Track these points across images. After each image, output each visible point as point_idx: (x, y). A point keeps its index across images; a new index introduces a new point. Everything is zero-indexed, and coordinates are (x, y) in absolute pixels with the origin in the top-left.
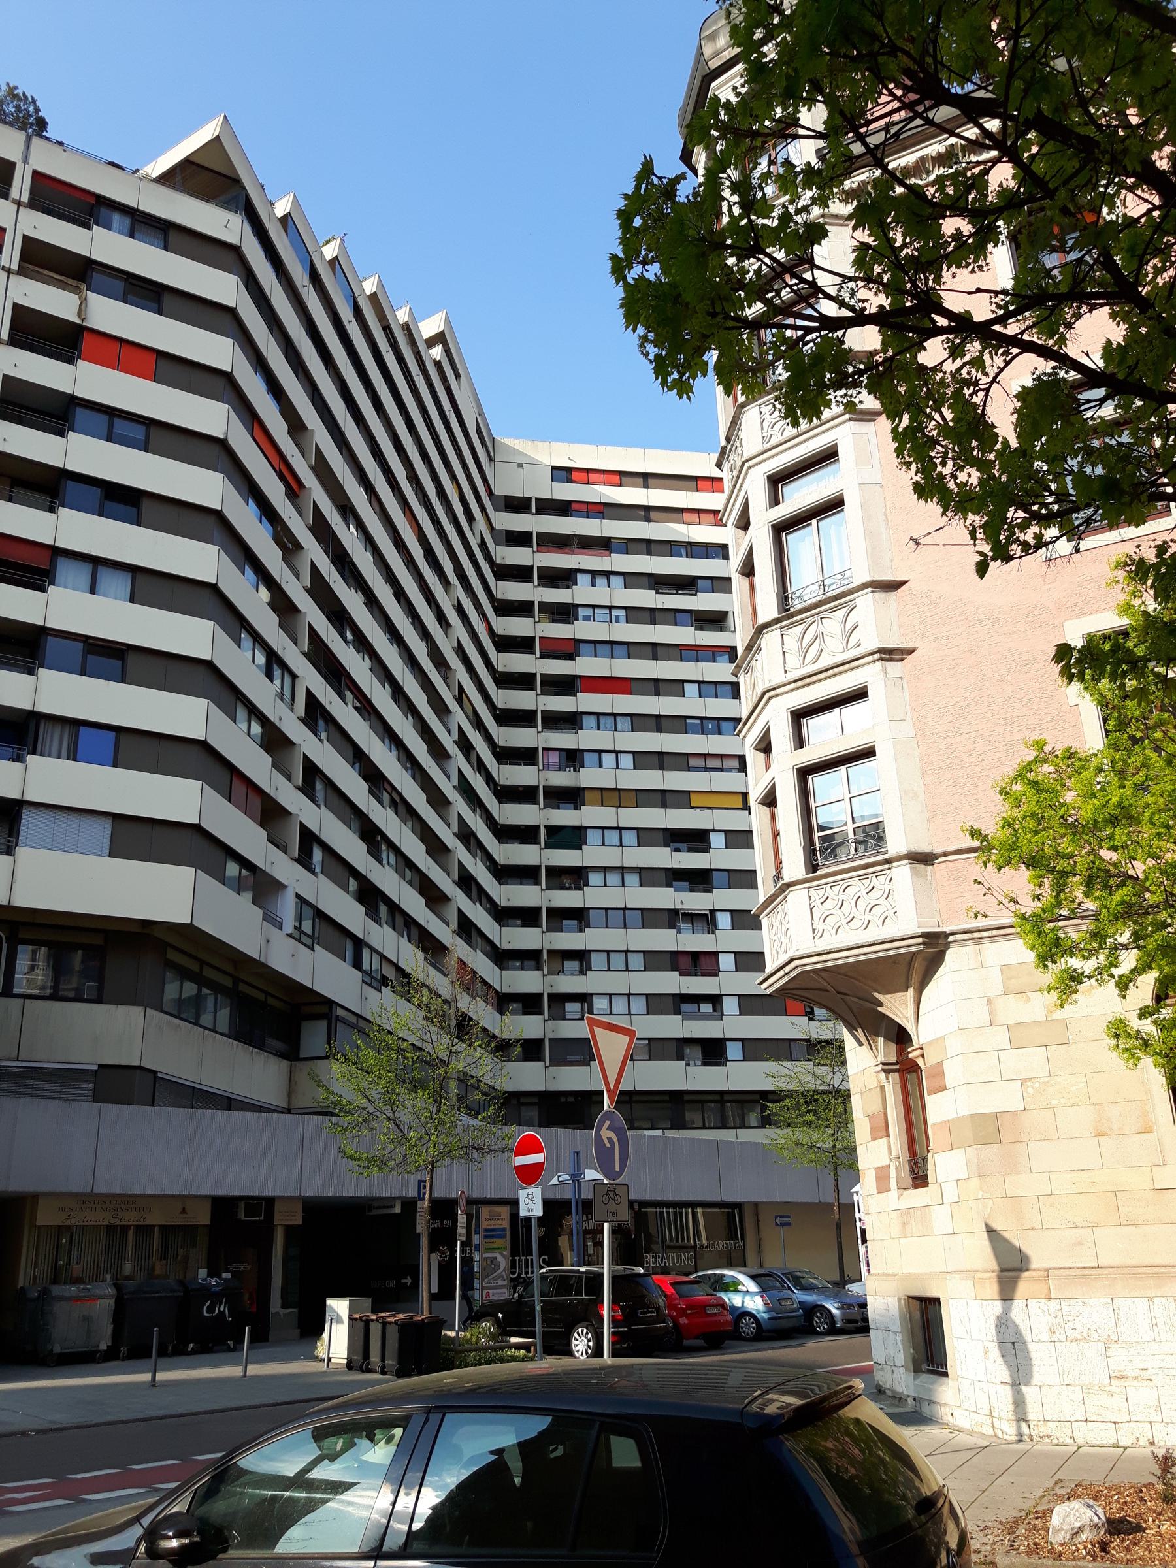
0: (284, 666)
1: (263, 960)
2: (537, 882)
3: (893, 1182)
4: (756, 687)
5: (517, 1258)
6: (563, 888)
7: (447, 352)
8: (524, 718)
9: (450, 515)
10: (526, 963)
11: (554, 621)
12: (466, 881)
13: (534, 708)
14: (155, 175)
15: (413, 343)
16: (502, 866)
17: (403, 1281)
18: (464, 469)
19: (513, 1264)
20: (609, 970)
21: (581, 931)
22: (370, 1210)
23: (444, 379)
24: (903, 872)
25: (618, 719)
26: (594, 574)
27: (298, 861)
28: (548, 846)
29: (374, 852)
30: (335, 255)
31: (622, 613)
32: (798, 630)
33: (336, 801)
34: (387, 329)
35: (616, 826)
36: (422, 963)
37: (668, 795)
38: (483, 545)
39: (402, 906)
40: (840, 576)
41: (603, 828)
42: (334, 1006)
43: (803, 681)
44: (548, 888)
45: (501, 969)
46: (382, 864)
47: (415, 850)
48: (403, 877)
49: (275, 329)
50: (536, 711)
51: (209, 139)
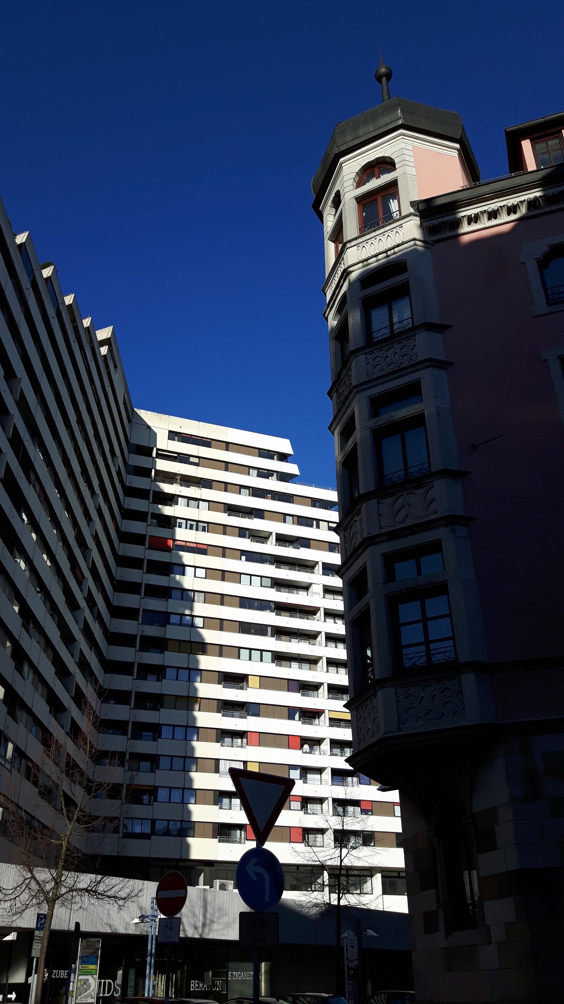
2: (125, 733)
3: (441, 925)
6: (145, 708)
7: (110, 350)
11: (160, 526)
13: (135, 633)
17: (9, 996)
18: (112, 423)
20: (171, 770)
21: (154, 740)
23: (107, 367)
26: (189, 498)
28: (148, 572)
29: (19, 669)
30: (48, 276)
31: (184, 522)
32: (389, 500)
35: (186, 667)
37: (225, 597)
38: (119, 473)
40: (420, 467)
41: (178, 668)
43: (392, 535)
46: (23, 678)
47: (54, 634)
48: (36, 689)
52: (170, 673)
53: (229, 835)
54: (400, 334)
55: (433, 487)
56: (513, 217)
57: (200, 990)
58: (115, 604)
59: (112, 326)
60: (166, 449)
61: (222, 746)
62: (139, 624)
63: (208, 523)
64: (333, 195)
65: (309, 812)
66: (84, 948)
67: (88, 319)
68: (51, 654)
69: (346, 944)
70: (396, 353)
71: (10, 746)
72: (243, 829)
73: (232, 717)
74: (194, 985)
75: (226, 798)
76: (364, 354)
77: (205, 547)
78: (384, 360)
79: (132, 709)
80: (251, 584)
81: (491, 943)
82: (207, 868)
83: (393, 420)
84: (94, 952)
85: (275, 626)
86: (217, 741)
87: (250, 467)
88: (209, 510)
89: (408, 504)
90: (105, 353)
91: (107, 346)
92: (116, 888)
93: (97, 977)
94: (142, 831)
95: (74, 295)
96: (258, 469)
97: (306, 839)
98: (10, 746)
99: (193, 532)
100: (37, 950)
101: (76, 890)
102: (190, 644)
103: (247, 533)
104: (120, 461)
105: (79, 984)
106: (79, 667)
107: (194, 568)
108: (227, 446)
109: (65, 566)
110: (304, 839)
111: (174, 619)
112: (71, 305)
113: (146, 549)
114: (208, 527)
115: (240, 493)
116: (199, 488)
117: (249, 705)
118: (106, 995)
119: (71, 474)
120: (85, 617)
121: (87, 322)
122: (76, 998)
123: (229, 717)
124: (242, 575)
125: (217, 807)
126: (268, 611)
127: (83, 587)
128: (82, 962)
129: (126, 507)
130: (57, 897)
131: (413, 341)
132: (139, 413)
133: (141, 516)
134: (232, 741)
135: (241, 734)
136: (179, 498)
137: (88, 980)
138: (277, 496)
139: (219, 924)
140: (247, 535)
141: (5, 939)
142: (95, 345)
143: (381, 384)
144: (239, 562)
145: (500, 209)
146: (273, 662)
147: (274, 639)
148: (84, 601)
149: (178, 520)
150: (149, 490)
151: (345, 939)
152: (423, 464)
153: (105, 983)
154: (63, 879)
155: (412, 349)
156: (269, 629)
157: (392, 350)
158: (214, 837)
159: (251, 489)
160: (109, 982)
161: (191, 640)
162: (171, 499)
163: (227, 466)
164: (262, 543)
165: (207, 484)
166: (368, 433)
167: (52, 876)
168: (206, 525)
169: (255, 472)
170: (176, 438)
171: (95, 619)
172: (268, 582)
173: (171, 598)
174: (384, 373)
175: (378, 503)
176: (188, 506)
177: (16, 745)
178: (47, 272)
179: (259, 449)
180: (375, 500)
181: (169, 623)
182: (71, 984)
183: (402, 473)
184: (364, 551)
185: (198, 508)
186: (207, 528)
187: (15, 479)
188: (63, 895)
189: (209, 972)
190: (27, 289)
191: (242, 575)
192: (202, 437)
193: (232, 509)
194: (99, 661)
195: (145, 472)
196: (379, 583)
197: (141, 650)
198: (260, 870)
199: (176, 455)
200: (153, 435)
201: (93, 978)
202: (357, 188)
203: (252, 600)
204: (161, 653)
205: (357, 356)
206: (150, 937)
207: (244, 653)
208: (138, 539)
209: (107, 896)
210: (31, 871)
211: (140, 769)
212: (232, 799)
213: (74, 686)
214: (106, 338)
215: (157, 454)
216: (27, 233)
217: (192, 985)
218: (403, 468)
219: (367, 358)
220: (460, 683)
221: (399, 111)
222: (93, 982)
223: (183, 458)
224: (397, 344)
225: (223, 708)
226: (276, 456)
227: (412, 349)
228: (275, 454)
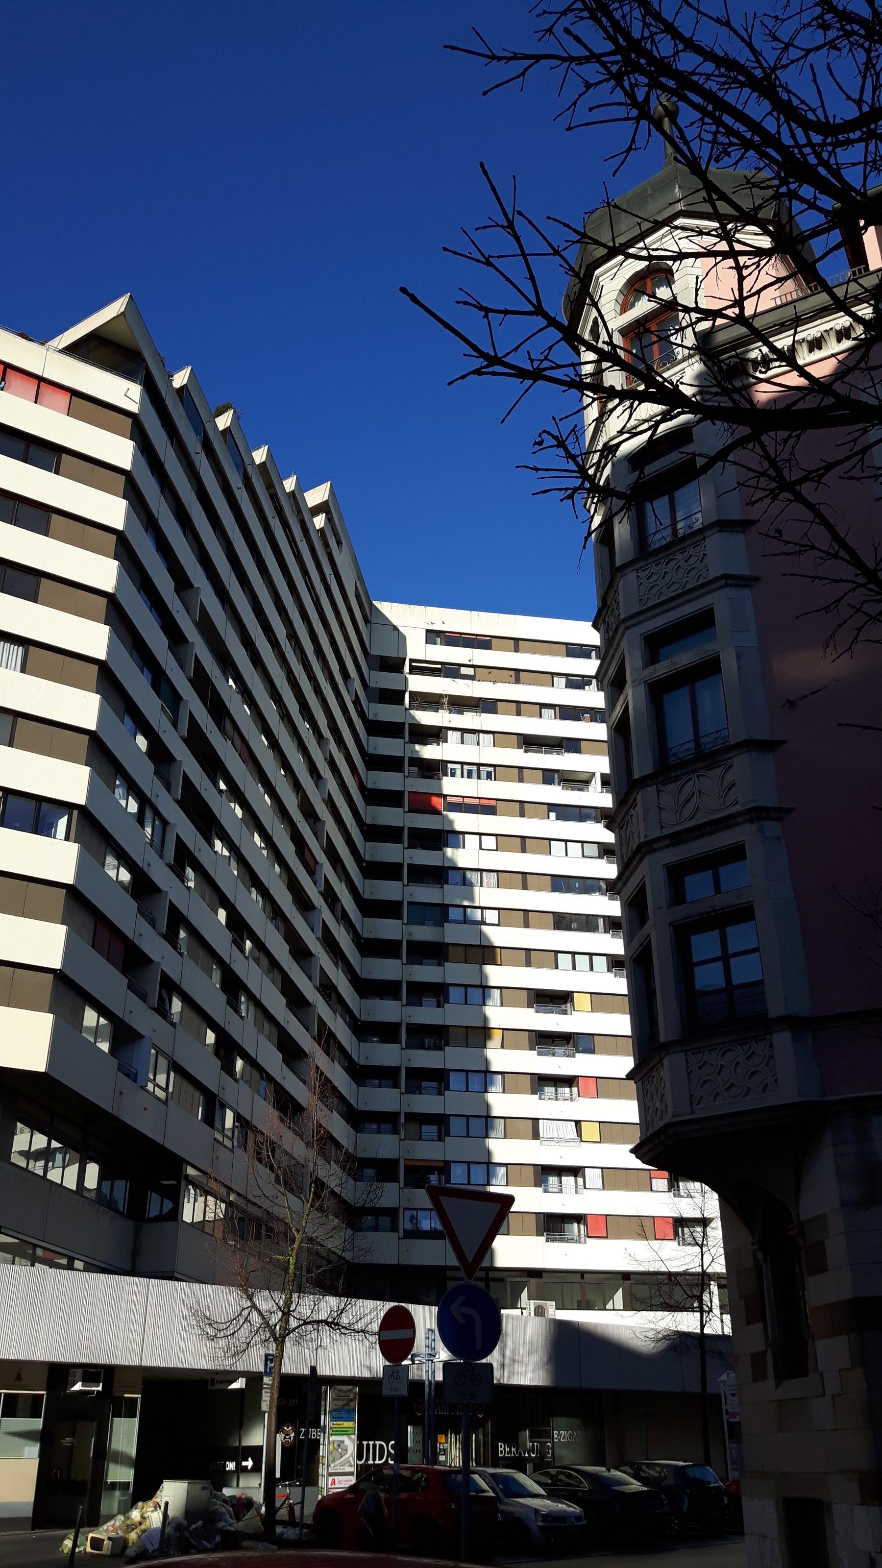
0: (157, 814)
1: (115, 1113)
2: (398, 998)
4: (631, 843)
5: (365, 1443)
6: (422, 1047)
7: (329, 520)
8: (390, 871)
9: (327, 673)
10: (383, 1126)
11: (424, 777)
12: (326, 1038)
14: (61, 347)
15: (299, 511)
16: (363, 1022)
17: (244, 1464)
19: (360, 1448)
20: (468, 1136)
22: (213, 1384)
24: (782, 1039)
25: (485, 874)
26: (464, 731)
27: (165, 937)
28: (411, 846)
29: (234, 1004)
30: (227, 426)
32: (674, 787)
33: (202, 954)
34: (274, 497)
35: (478, 983)
36: (276, 1122)
38: (357, 702)
39: (259, 1061)
41: (466, 986)
42: (184, 1165)
43: (677, 838)
44: (408, 1047)
45: (360, 1041)
47: (280, 950)
48: (261, 1030)
49: (167, 493)
50: (402, 865)
51: (115, 315)
52: (455, 994)
53: (562, 1230)
54: (685, 537)
55: (732, 765)
56: (847, 344)
57: (513, 1455)
58: (367, 896)
59: (329, 482)
60: (423, 658)
61: (540, 1098)
62: (403, 924)
63: (494, 766)
64: (590, 323)
65: (682, 1194)
66: (334, 1399)
67: (291, 479)
68: (278, 978)
69: (724, 1391)
70: (679, 567)
71: (229, 1116)
72: (582, 1221)
73: (553, 1055)
74: (503, 1449)
75: (553, 1175)
76: (634, 570)
77: (493, 803)
78: (663, 578)
79: (404, 1049)
80: (567, 855)
81: (824, 1395)
82: (532, 1280)
83: (676, 669)
84: (347, 1404)
85: (609, 917)
86: (534, 1092)
87: (553, 674)
88: (494, 746)
89: (699, 791)
90: (322, 525)
91: (324, 514)
92: (366, 1320)
93: (354, 1437)
94: (433, 1226)
95: (267, 447)
96: (567, 675)
97: (680, 1235)
98: (229, 1116)
99: (474, 781)
100: (266, 1401)
101: (310, 1323)
102: (481, 949)
103: (556, 776)
104: (357, 684)
105: (331, 1447)
106: (319, 992)
107: (478, 836)
108: (516, 644)
109: (288, 850)
110: (676, 1234)
111: (454, 914)
112: (264, 463)
113: (405, 812)
114: (494, 772)
115: (541, 716)
116: (478, 714)
117: (577, 1037)
118: (377, 1462)
119: (285, 715)
120: (323, 920)
121: (289, 484)
122: (329, 1466)
123: (548, 1055)
124: (552, 842)
125: (540, 1190)
126: (597, 893)
127: (316, 876)
128: (333, 1418)
129: (371, 751)
130: (286, 1331)
131: (702, 549)
132: (379, 608)
133: (393, 764)
134: (556, 1091)
135: (569, 1081)
136: (449, 732)
137: (343, 1442)
138: (599, 716)
139: (525, 1364)
140: (556, 780)
141: (230, 1387)
142: (303, 515)
143: (659, 615)
144: (546, 821)
145: (825, 335)
146: (609, 970)
147: (608, 936)
148: (321, 897)
149: (450, 766)
150: (403, 724)
151: (722, 1385)
152: (719, 731)
153: (374, 1446)
154: (292, 1308)
155: (701, 561)
156: (601, 921)
157: (672, 564)
158: (539, 1234)
159: (557, 708)
160: (380, 1445)
161: (483, 944)
162: (436, 734)
163: (517, 675)
164: (581, 790)
165: (488, 706)
166: (642, 688)
167: (277, 1304)
168: (492, 769)
169: (563, 681)
170: (438, 640)
171: (339, 921)
172: (593, 850)
173: (448, 884)
174: (663, 598)
175: (658, 791)
176: (462, 743)
177: (238, 1113)
178: (223, 421)
179: (567, 644)
180: (655, 787)
181: (447, 920)
182: (321, 1446)
183: (692, 745)
184: (642, 859)
185: (478, 744)
186: (493, 773)
187: (205, 735)
188: (294, 1330)
189: (525, 1430)
190: (197, 453)
191: (552, 842)
192: (477, 635)
193: (530, 742)
194: (350, 981)
195: (395, 697)
196: (661, 907)
197: (409, 962)
198: (469, 1311)
199: (440, 666)
200: (400, 639)
201: (350, 1439)
202: (621, 314)
203: (571, 880)
204: (439, 965)
205: (625, 574)
206: (427, 1383)
207: (564, 960)
208: (392, 798)
209: (354, 1330)
210: (250, 1297)
211: (423, 1137)
212: (563, 1178)
213: (316, 1022)
214: (321, 501)
215: (411, 667)
216: (189, 369)
217: (500, 1449)
218: (693, 738)
219: (638, 577)
220: (771, 1046)
221: (677, 190)
222: (350, 1444)
223: (450, 670)
224: (680, 553)
225: (539, 1043)
226: (594, 652)
227: (701, 561)
228: (593, 650)
